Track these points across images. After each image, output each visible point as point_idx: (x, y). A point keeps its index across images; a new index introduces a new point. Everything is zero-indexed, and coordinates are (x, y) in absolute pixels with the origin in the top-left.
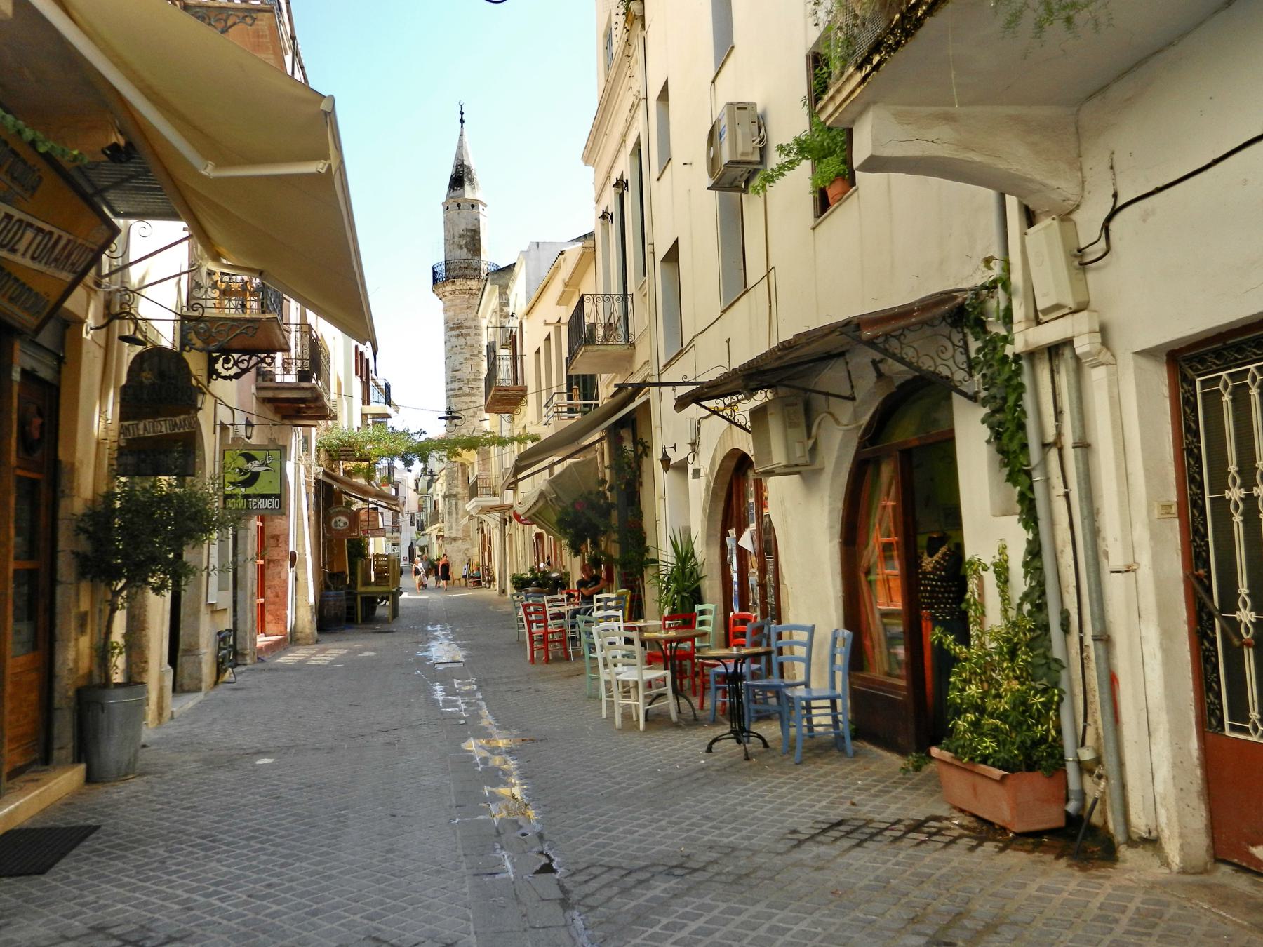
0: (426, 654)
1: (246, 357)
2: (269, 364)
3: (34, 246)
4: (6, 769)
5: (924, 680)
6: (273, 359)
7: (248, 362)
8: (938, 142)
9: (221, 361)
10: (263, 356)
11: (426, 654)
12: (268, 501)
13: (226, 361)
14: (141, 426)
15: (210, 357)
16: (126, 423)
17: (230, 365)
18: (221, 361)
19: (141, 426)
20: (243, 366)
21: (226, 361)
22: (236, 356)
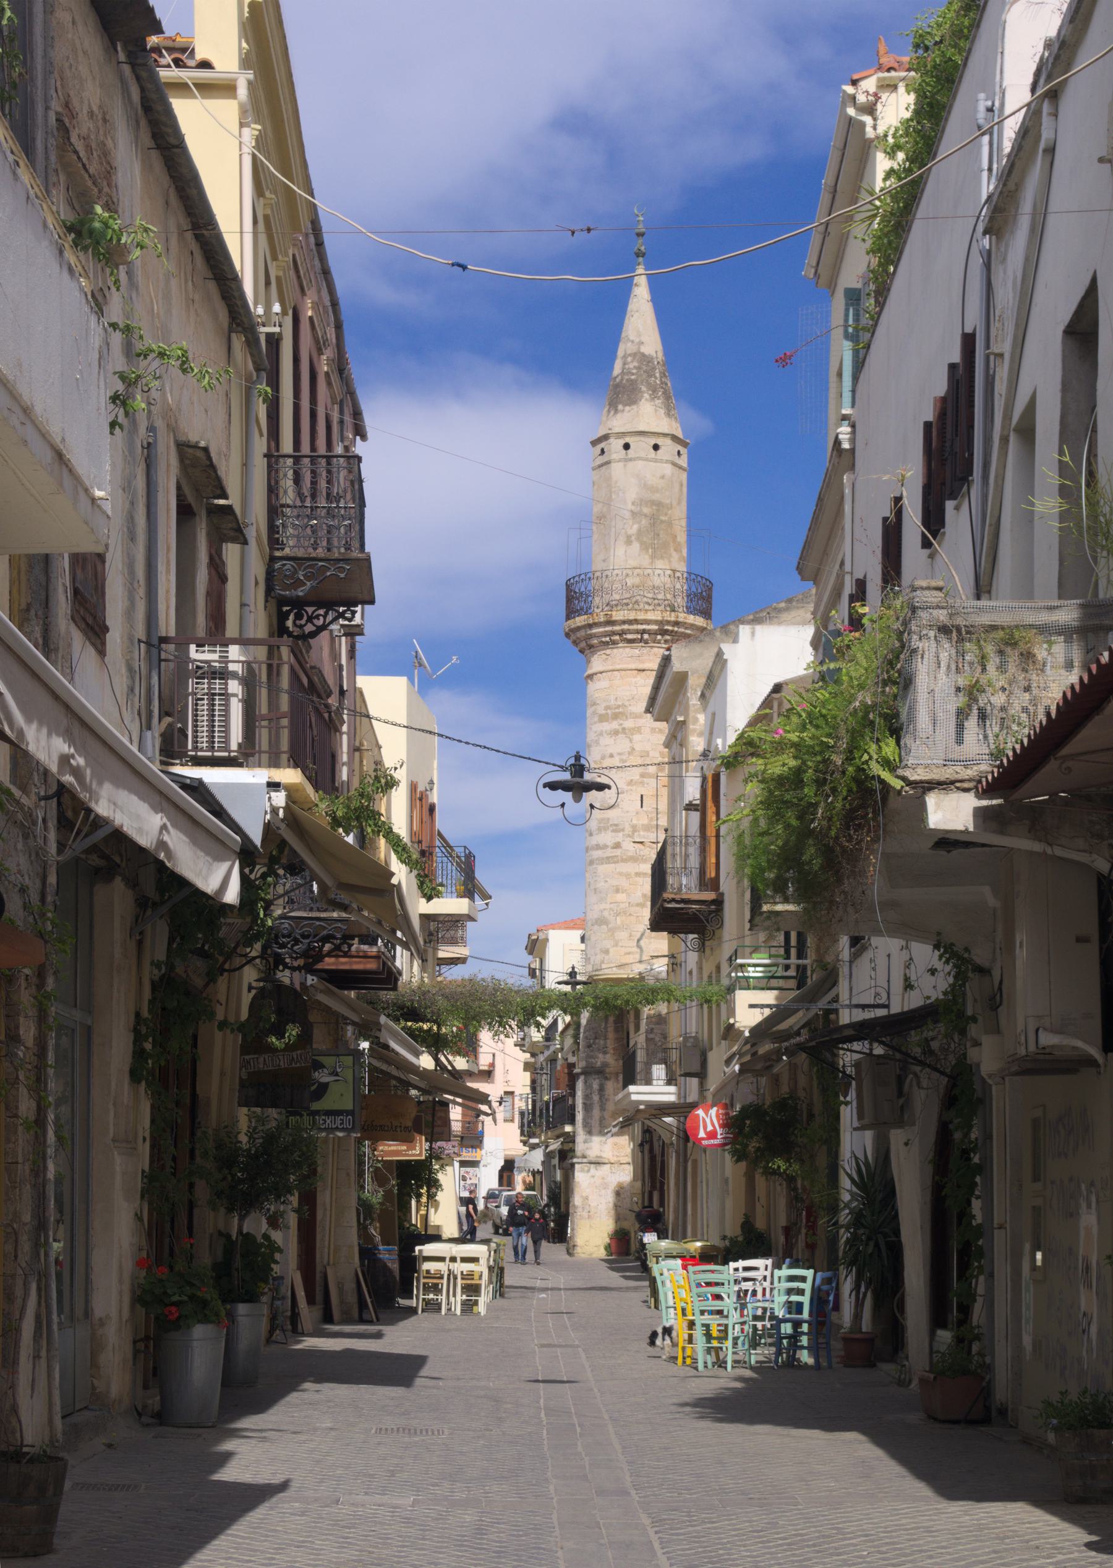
0: (985, 803)
1: (322, 612)
2: (350, 620)
3: (327, 1238)
4: (567, 1257)
5: (896, 1250)
6: (354, 613)
7: (325, 617)
8: (999, 55)
9: (291, 617)
10: (341, 609)
11: (985, 803)
12: (338, 1119)
13: (299, 616)
14: (261, 1060)
15: (279, 611)
16: (247, 1057)
17: (303, 622)
18: (291, 617)
19: (261, 1060)
20: (320, 622)
21: (299, 616)
22: (310, 610)
